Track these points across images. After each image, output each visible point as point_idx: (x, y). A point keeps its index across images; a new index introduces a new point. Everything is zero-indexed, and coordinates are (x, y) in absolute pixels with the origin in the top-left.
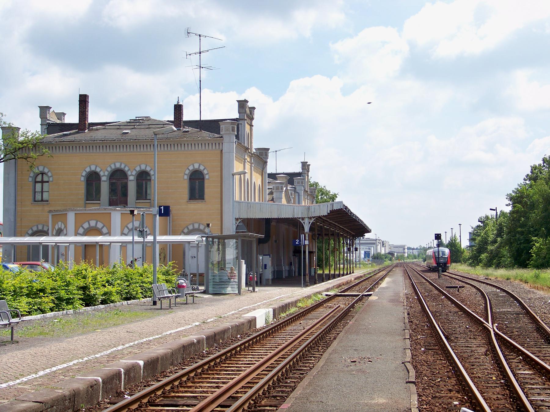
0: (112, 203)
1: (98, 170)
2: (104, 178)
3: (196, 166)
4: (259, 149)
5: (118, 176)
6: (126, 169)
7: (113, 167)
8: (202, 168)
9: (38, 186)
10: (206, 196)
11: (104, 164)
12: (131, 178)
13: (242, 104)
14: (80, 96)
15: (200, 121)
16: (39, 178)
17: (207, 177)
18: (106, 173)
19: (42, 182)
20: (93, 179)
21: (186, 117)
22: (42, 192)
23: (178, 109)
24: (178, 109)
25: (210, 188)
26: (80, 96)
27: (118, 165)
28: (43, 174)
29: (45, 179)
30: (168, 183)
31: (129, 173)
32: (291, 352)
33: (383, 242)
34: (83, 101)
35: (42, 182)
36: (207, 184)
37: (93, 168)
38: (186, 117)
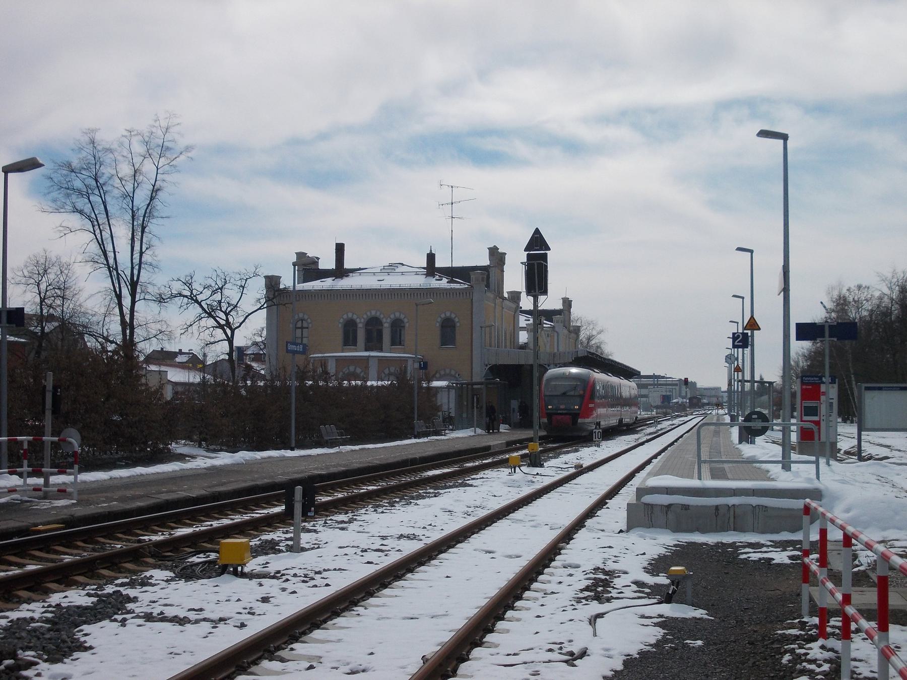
2: (360, 325)
3: (448, 314)
17: (458, 324)
19: (302, 328)
21: (438, 264)
29: (305, 325)
31: (384, 320)
38: (438, 264)
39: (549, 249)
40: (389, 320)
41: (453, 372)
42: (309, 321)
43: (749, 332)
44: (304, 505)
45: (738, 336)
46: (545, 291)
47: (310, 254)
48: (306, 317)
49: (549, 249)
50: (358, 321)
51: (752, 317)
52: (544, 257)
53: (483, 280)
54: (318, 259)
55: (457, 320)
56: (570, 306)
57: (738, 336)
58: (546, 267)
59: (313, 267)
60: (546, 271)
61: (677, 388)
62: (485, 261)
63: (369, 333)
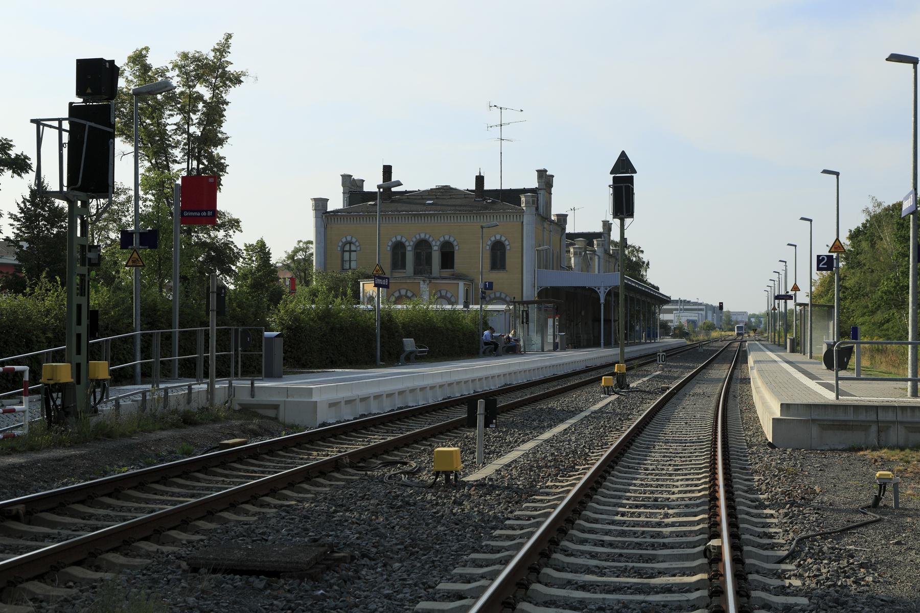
0: (417, 272)
1: (404, 240)
2: (409, 248)
3: (498, 237)
4: (557, 215)
5: (423, 246)
6: (431, 239)
7: (418, 237)
8: (503, 239)
9: (347, 255)
10: (507, 266)
11: (409, 232)
12: (435, 248)
13: (542, 174)
14: (384, 166)
15: (501, 190)
16: (347, 248)
17: (508, 248)
18: (412, 243)
19: (350, 251)
20: (398, 248)
21: (487, 187)
22: (350, 261)
23: (480, 180)
24: (480, 180)
25: (511, 259)
26: (384, 166)
27: (423, 236)
28: (350, 243)
29: (353, 248)
30: (473, 256)
31: (434, 243)
32: (630, 543)
33: (778, 297)
34: (387, 170)
35: (350, 251)
36: (508, 254)
37: (399, 238)
38: (487, 187)
39: (635, 172)
40: (438, 243)
41: (503, 296)
42: (357, 244)
43: (835, 255)
44: (486, 418)
45: (823, 259)
46: (631, 215)
47: (356, 177)
48: (354, 240)
49: (635, 172)
50: (407, 244)
51: (837, 239)
52: (631, 180)
53: (533, 203)
54: (363, 181)
55: (507, 243)
56: (610, 230)
57: (823, 259)
58: (633, 189)
59: (358, 190)
60: (633, 194)
61: (703, 313)
62: (533, 183)
63: (417, 256)
